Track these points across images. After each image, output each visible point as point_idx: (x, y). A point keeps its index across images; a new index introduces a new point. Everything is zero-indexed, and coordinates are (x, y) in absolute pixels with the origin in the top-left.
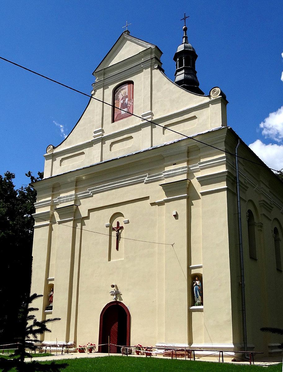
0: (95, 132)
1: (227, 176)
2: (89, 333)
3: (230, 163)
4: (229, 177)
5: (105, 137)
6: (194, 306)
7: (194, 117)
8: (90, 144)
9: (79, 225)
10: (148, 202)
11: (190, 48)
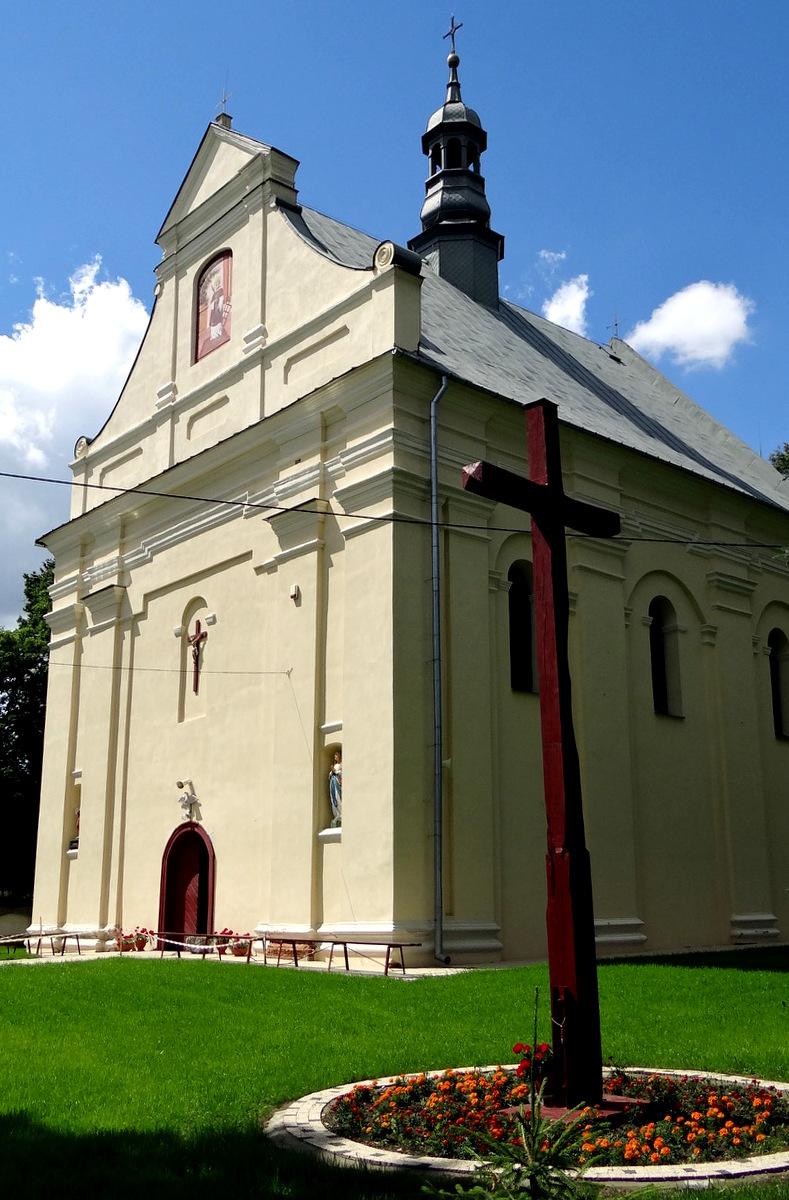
0: (160, 394)
1: (394, 482)
2: (143, 909)
3: (416, 445)
4: (400, 483)
5: (181, 402)
6: (330, 827)
7: (344, 331)
8: (149, 428)
9: (128, 634)
10: (251, 564)
11: (458, 114)
